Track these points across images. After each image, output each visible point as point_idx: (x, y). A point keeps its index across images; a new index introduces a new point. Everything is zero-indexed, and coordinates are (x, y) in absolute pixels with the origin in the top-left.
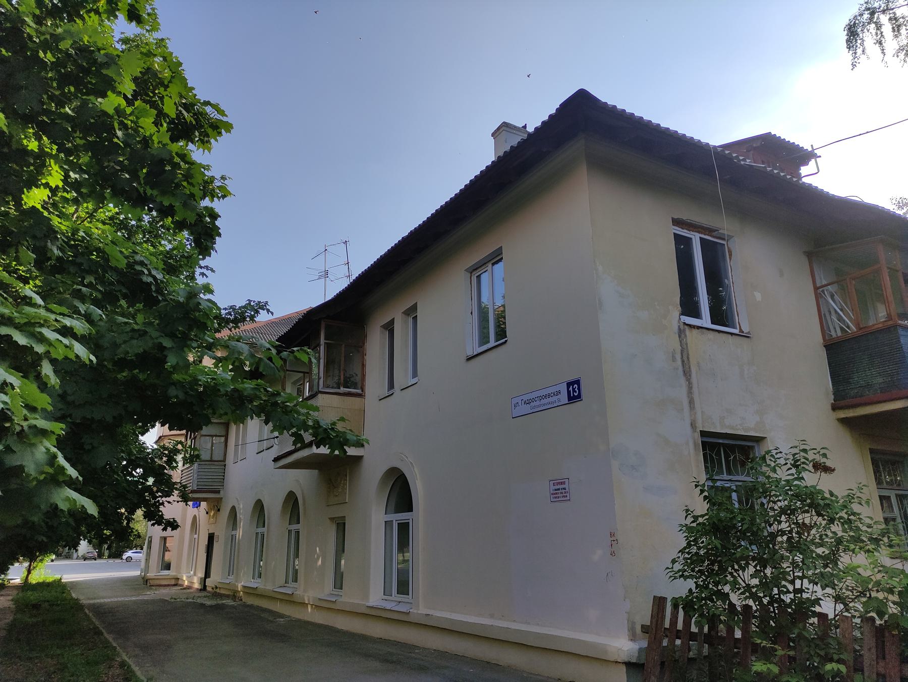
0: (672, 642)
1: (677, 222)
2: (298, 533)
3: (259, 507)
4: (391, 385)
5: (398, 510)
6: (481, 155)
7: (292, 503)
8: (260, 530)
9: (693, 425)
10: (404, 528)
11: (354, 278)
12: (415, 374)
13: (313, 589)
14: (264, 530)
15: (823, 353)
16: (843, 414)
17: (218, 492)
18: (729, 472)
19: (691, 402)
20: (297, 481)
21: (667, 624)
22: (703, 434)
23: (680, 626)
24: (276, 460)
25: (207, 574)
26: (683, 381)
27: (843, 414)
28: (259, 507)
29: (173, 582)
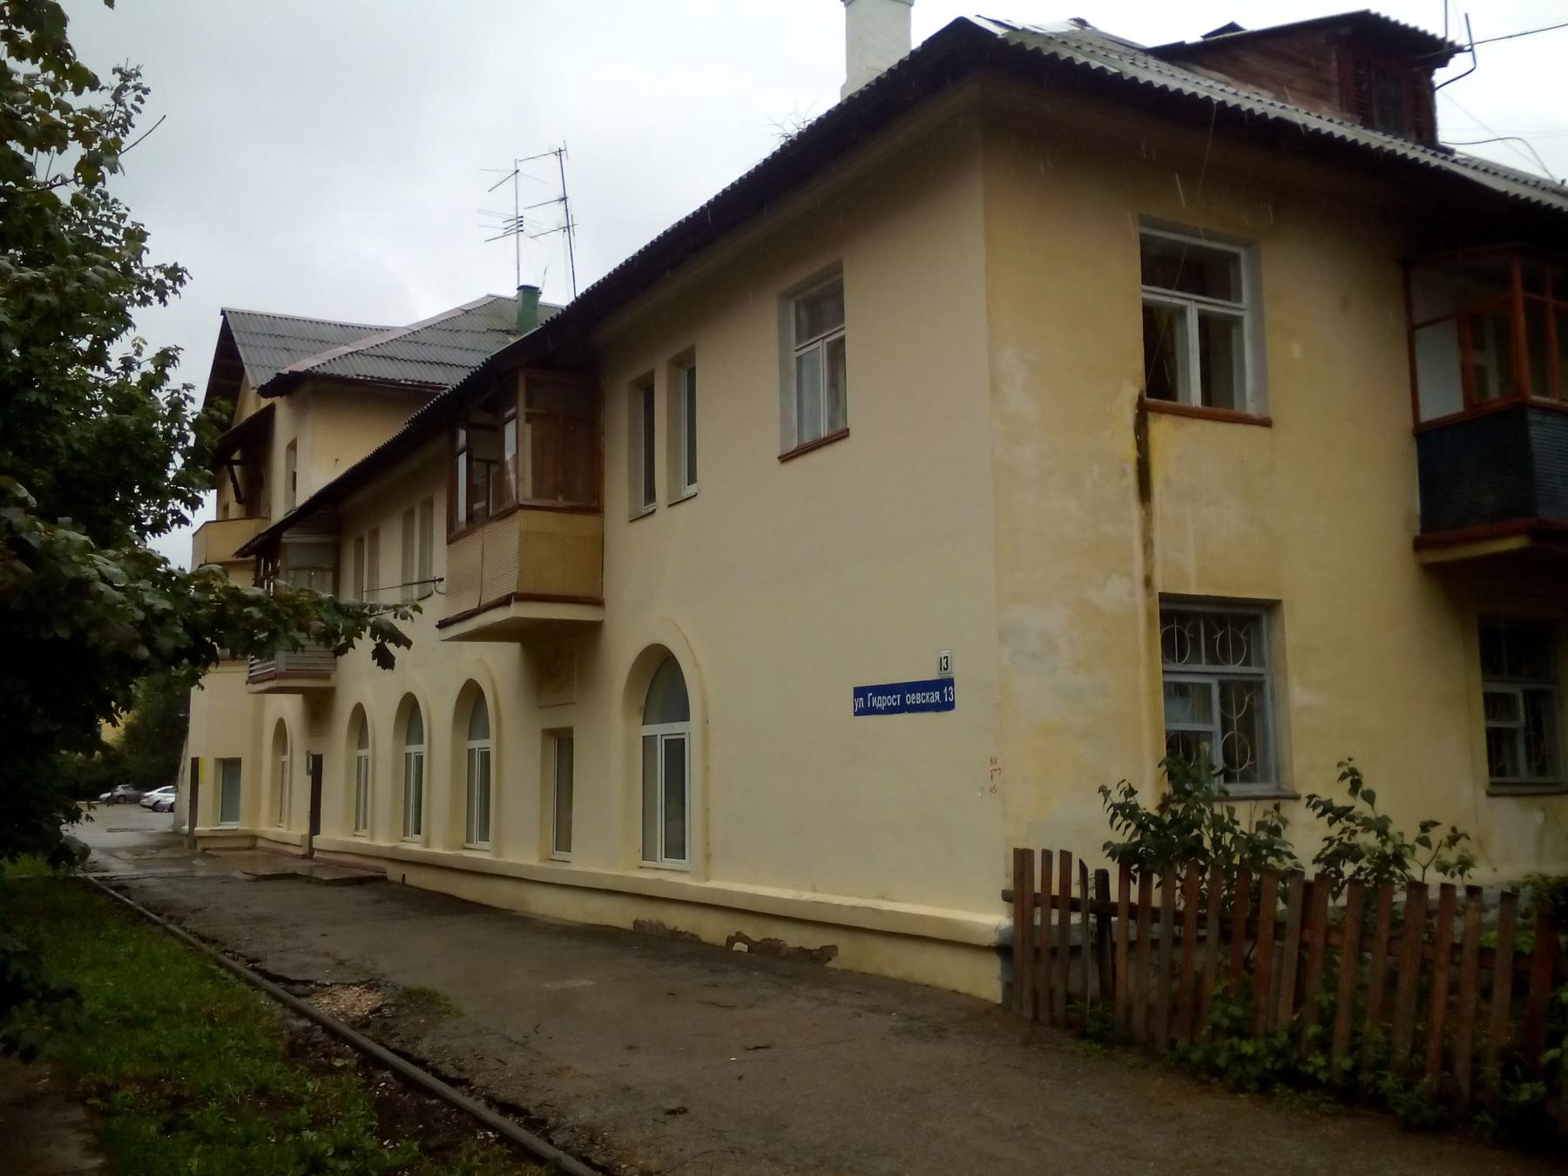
0: (1064, 920)
4: (650, 495)
5: (666, 718)
6: (809, 80)
7: (472, 699)
8: (413, 749)
9: (1148, 582)
10: (676, 748)
12: (692, 479)
13: (518, 845)
14: (423, 748)
16: (1431, 557)
17: (327, 677)
19: (1148, 543)
21: (1038, 888)
22: (1164, 598)
23: (1055, 891)
24: (443, 625)
25: (315, 827)
26: (1134, 510)
27: (1431, 557)
29: (246, 843)
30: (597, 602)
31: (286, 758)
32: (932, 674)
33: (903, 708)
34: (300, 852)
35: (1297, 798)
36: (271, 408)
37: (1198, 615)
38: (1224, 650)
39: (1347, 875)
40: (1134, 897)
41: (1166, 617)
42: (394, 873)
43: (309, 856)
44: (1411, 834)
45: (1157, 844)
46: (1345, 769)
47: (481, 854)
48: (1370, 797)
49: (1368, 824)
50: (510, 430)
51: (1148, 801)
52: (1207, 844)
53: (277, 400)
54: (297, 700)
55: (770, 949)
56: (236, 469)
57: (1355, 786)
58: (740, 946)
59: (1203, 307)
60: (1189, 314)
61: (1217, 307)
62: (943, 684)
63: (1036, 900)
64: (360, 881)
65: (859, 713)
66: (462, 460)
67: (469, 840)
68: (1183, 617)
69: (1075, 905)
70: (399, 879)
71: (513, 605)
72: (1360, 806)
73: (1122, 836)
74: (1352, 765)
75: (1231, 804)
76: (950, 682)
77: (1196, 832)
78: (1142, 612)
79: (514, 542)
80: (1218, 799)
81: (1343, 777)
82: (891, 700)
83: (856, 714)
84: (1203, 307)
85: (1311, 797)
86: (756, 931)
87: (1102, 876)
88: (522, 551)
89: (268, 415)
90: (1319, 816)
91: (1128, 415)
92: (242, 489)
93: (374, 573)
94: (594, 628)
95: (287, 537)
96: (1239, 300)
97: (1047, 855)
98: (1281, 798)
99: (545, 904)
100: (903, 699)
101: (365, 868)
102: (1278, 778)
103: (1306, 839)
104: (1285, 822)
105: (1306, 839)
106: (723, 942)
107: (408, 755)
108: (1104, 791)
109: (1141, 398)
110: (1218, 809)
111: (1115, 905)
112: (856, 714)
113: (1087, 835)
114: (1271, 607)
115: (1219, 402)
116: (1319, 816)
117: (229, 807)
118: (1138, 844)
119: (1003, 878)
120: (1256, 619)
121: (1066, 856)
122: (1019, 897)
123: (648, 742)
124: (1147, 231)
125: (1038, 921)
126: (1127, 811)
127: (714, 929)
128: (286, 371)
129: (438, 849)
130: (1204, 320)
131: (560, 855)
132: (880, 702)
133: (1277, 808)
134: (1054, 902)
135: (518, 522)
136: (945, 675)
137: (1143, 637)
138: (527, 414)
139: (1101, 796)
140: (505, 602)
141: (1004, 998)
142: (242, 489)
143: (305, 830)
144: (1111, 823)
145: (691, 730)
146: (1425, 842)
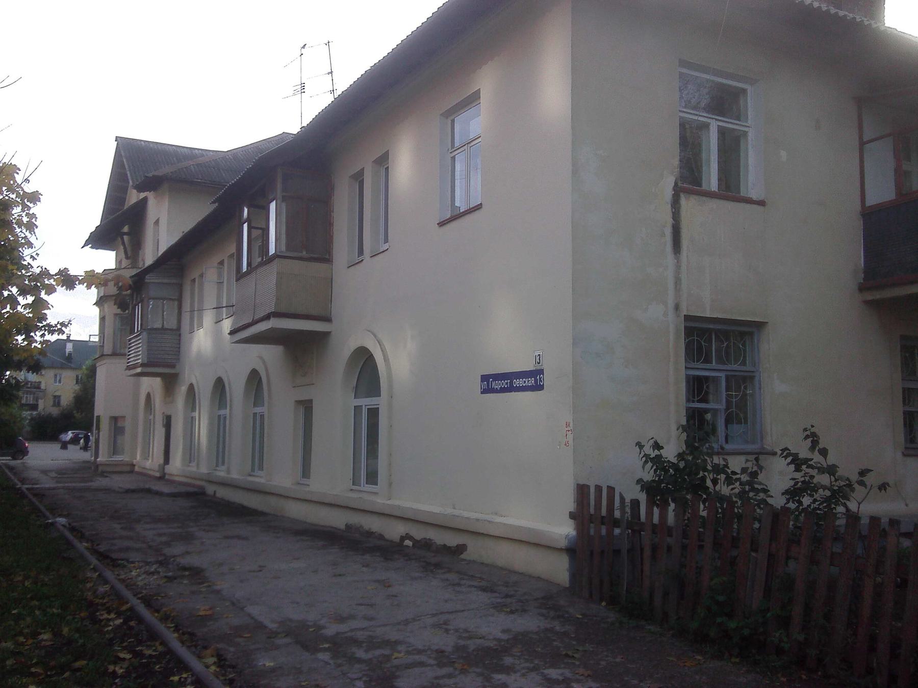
0: (610, 533)
1: (683, 63)
2: (262, 416)
3: (220, 386)
4: (361, 252)
7: (254, 378)
9: (677, 307)
10: (373, 413)
11: (339, 92)
12: (386, 241)
13: (281, 475)
15: (860, 224)
16: (869, 296)
17: (173, 366)
18: (720, 361)
20: (261, 358)
21: (592, 511)
22: (688, 318)
23: (604, 512)
26: (670, 258)
27: (869, 296)
28: (220, 386)
29: (128, 469)
30: (327, 319)
31: (152, 417)
32: (529, 366)
33: (511, 389)
34: (158, 475)
35: (775, 454)
36: (145, 200)
37: (709, 331)
38: (727, 353)
39: (805, 505)
40: (656, 519)
41: (689, 331)
42: (210, 489)
43: (162, 478)
44: (854, 477)
45: (673, 482)
46: (808, 433)
47: (260, 479)
48: (824, 452)
49: (821, 470)
50: (273, 206)
51: (670, 453)
52: (709, 483)
53: (150, 195)
54: (158, 380)
55: (426, 545)
56: (125, 237)
57: (815, 443)
58: (408, 543)
59: (721, 124)
60: (711, 128)
61: (730, 124)
62: (537, 373)
63: (591, 518)
64: (188, 495)
65: (484, 392)
66: (246, 225)
67: (253, 470)
68: (703, 332)
69: (616, 523)
70: (212, 493)
71: (272, 319)
72: (817, 458)
73: (648, 475)
74: (813, 430)
75: (726, 457)
76: (541, 372)
77: (701, 474)
78: (672, 329)
79: (273, 279)
80: (718, 454)
81: (807, 437)
82: (504, 384)
83: (482, 393)
84: (721, 124)
85: (783, 450)
86: (419, 533)
87: (635, 503)
88: (278, 284)
89: (143, 203)
90: (788, 464)
91: (669, 192)
92: (129, 249)
93: (201, 301)
94: (326, 335)
95: (149, 279)
96: (746, 120)
97: (599, 489)
98: (759, 455)
99: (296, 511)
100: (511, 383)
101: (194, 486)
102: (762, 440)
103: (778, 478)
104: (761, 468)
105: (778, 478)
106: (398, 540)
107: (255, 414)
108: (640, 445)
109: (676, 184)
110: (716, 460)
111: (643, 524)
112: (482, 393)
113: (626, 474)
114: (760, 325)
115: (730, 189)
116: (788, 464)
117: (115, 449)
118: (660, 481)
119: (569, 503)
120: (751, 334)
121: (611, 490)
122: (580, 516)
123: (358, 409)
124: (684, 71)
125: (592, 532)
126: (658, 461)
127: (395, 531)
128: (150, 175)
129: (235, 475)
130: (722, 132)
131: (305, 481)
132: (497, 385)
133: (757, 459)
134: (603, 521)
135: (274, 267)
136: (538, 368)
137: (673, 344)
138: (283, 197)
139: (637, 449)
140: (267, 317)
141: (570, 581)
142: (129, 249)
143: (162, 461)
144: (643, 467)
145: (381, 402)
146: (862, 483)
